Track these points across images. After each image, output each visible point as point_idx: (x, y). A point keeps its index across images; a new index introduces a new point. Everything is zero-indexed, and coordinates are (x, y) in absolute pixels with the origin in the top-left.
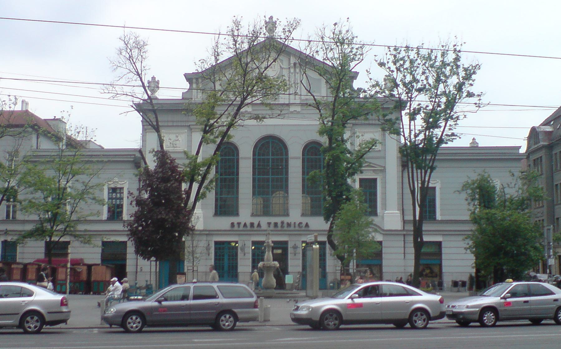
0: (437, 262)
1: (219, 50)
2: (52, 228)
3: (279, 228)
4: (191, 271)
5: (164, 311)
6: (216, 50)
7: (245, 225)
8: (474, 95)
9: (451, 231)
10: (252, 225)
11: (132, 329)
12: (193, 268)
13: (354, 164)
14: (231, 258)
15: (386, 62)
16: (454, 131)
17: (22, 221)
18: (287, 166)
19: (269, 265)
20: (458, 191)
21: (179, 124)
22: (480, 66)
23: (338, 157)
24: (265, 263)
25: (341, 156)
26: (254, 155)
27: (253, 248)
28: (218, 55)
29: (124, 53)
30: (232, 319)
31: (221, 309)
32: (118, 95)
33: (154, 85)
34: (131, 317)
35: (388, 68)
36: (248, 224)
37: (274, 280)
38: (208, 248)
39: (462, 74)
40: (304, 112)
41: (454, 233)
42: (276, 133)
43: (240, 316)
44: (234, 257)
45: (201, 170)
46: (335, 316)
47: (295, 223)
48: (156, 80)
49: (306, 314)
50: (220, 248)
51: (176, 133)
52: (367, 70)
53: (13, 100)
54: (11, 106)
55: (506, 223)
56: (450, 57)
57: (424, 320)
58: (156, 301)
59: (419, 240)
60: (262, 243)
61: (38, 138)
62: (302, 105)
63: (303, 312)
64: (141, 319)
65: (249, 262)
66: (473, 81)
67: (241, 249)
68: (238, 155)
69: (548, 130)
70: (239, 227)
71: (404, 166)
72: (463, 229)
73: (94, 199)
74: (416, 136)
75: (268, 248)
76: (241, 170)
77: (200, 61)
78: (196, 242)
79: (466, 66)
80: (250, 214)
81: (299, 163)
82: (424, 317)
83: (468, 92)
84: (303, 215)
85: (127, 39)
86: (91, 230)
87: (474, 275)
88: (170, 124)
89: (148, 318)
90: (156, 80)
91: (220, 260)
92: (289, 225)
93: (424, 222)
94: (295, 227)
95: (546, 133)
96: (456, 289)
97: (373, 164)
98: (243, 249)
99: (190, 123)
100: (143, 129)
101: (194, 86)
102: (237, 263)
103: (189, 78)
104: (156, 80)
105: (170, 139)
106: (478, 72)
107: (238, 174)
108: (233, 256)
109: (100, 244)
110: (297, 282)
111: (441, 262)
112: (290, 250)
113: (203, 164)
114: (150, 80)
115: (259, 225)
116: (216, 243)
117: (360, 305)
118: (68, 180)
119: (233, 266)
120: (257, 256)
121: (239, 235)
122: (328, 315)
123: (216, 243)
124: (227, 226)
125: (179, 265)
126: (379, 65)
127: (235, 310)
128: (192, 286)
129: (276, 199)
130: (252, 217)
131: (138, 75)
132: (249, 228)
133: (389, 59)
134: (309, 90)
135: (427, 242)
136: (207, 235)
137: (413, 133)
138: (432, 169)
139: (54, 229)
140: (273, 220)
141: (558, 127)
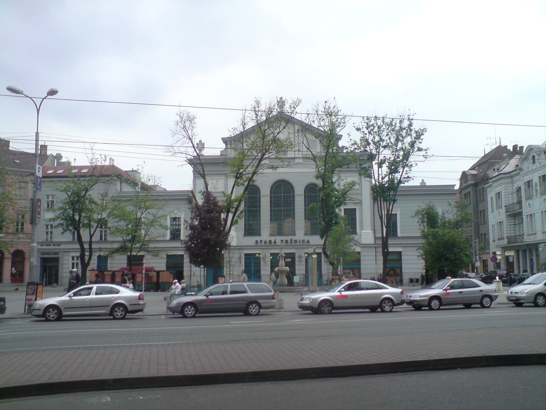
0: (399, 266)
1: (246, 121)
3: (289, 244)
7: (265, 242)
8: (423, 149)
10: (270, 242)
11: (188, 316)
12: (230, 272)
15: (361, 127)
16: (409, 175)
17: (111, 241)
19: (282, 270)
24: (280, 268)
26: (271, 193)
27: (271, 258)
28: (245, 125)
29: (180, 124)
30: (257, 307)
32: (176, 154)
33: (201, 146)
36: (268, 242)
37: (286, 280)
38: (240, 258)
39: (414, 135)
40: (305, 163)
41: (413, 245)
42: (286, 178)
43: (262, 305)
45: (234, 205)
47: (300, 240)
49: (309, 303)
50: (248, 258)
51: (217, 179)
52: (348, 134)
53: (104, 158)
55: (446, 238)
56: (406, 124)
58: (204, 296)
59: (386, 251)
60: (278, 254)
61: (121, 184)
62: (303, 158)
63: (306, 302)
64: (194, 308)
65: (269, 268)
66: (422, 140)
69: (474, 173)
70: (261, 243)
71: (375, 199)
73: (161, 225)
74: (383, 179)
79: (417, 130)
82: (390, 304)
83: (418, 148)
87: (424, 274)
88: (213, 173)
89: (199, 308)
92: (296, 241)
94: (300, 243)
96: (412, 284)
98: (264, 259)
99: (226, 172)
101: (229, 146)
102: (260, 269)
105: (213, 183)
106: (425, 133)
109: (165, 256)
112: (297, 259)
113: (236, 200)
114: (198, 142)
115: (275, 242)
116: (246, 255)
117: (346, 296)
120: (274, 264)
122: (323, 304)
123: (246, 255)
127: (259, 301)
128: (229, 285)
129: (287, 223)
132: (268, 244)
133: (363, 126)
137: (380, 177)
139: (133, 246)
140: (285, 238)
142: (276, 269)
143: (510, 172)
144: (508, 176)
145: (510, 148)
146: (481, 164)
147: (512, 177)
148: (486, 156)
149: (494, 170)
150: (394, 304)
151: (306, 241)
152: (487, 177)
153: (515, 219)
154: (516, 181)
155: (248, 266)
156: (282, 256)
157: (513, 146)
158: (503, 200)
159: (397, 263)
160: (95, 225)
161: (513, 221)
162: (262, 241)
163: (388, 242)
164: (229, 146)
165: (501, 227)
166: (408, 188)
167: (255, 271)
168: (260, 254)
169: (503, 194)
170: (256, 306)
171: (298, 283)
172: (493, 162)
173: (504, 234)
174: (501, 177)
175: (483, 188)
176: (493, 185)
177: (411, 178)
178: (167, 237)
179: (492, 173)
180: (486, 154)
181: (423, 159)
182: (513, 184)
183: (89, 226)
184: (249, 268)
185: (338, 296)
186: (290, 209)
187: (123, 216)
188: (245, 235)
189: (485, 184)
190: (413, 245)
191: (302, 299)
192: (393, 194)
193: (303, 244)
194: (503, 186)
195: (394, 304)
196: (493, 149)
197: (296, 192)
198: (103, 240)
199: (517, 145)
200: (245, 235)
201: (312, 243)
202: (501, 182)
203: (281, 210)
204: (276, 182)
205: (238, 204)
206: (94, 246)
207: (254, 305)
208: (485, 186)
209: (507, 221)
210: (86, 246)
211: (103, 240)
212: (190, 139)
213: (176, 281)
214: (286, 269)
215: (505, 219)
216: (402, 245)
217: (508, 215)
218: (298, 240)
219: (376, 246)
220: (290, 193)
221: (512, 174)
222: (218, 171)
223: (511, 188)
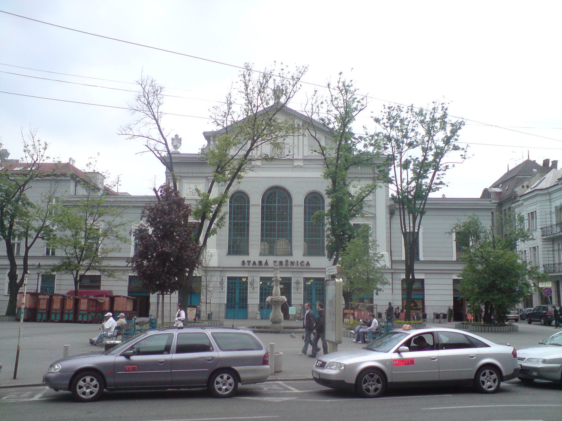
0: (421, 297)
1: (232, 100)
2: (79, 263)
3: (284, 266)
4: (205, 303)
5: (134, 369)
6: (229, 99)
7: (254, 263)
9: (433, 270)
10: (260, 263)
11: (84, 397)
12: (206, 300)
13: (354, 206)
15: (380, 118)
16: (442, 180)
17: (60, 257)
20: (449, 233)
21: (198, 175)
22: (464, 123)
23: (342, 198)
24: (273, 297)
25: (345, 198)
27: (261, 283)
28: (231, 103)
29: (143, 99)
30: (231, 380)
31: (218, 366)
32: (134, 137)
33: (177, 140)
34: (83, 378)
36: (257, 263)
37: (282, 314)
38: (221, 283)
39: (449, 128)
41: (448, 272)
43: (242, 376)
44: (245, 291)
45: (212, 208)
46: (376, 376)
47: (297, 262)
49: (337, 375)
50: (232, 283)
51: (195, 183)
52: (364, 127)
53: (43, 146)
54: (40, 150)
55: (501, 261)
56: (438, 115)
57: (494, 381)
58: (122, 355)
59: (411, 277)
60: (270, 279)
61: (76, 186)
62: (304, 160)
63: (331, 372)
64: (98, 381)
67: (250, 284)
68: (249, 202)
70: (249, 264)
71: (392, 213)
73: (117, 237)
74: (408, 184)
75: (277, 282)
76: (251, 215)
77: (213, 107)
79: (453, 122)
80: (258, 254)
81: (302, 210)
82: (494, 376)
83: (454, 145)
85: (144, 83)
87: (452, 308)
88: (190, 175)
89: (109, 380)
90: (179, 137)
91: (232, 293)
92: (292, 263)
93: (415, 262)
94: (297, 265)
95: (496, 193)
96: (437, 320)
98: (252, 284)
99: (207, 175)
101: (212, 143)
102: (247, 296)
103: (208, 136)
104: (179, 137)
105: (190, 188)
106: (462, 127)
107: (248, 219)
108: (243, 289)
109: (127, 279)
110: (299, 314)
111: (424, 297)
112: (293, 285)
113: (215, 201)
114: (174, 137)
115: (266, 263)
116: (229, 278)
117: (411, 361)
118: (94, 219)
119: (243, 298)
120: (265, 291)
121: (249, 271)
122: (367, 377)
123: (229, 278)
124: (239, 264)
125: (191, 298)
126: (375, 121)
127: (236, 368)
128: (175, 332)
129: (281, 244)
132: (257, 266)
134: (314, 136)
135: (418, 279)
136: (221, 271)
137: (405, 181)
138: (422, 213)
139: (81, 263)
140: (279, 259)
141: (507, 189)
142: (269, 299)
143: (547, 188)
144: (545, 192)
145: (540, 163)
146: (505, 182)
147: (550, 194)
148: (509, 172)
149: (523, 187)
150: (501, 378)
151: (305, 263)
152: (515, 194)
153: (553, 244)
154: (555, 199)
156: (277, 280)
157: (544, 161)
158: (538, 221)
159: (419, 293)
160: (34, 234)
161: (551, 246)
162: (250, 261)
164: (212, 143)
165: (535, 254)
167: (240, 299)
168: (247, 278)
169: (538, 214)
170: (228, 378)
172: (521, 178)
173: (539, 261)
174: (536, 193)
175: (510, 208)
176: (525, 204)
179: (519, 190)
180: (509, 170)
181: (460, 160)
182: (550, 202)
183: (26, 235)
185: (395, 360)
186: (286, 223)
187: (73, 226)
188: (229, 253)
189: (513, 203)
190: (448, 272)
191: (323, 365)
192: (421, 203)
194: (538, 205)
195: (501, 378)
196: (518, 165)
197: (294, 202)
198: (50, 255)
199: (549, 160)
200: (229, 253)
201: (312, 265)
202: (538, 199)
203: (275, 223)
205: (217, 207)
206: (30, 262)
207: (225, 376)
208: (513, 206)
209: (544, 246)
210: (19, 262)
211: (50, 255)
212: (155, 119)
213: (110, 314)
214: (282, 299)
215: (541, 243)
217: (544, 239)
218: (296, 261)
221: (550, 190)
222: (197, 173)
223: (549, 207)
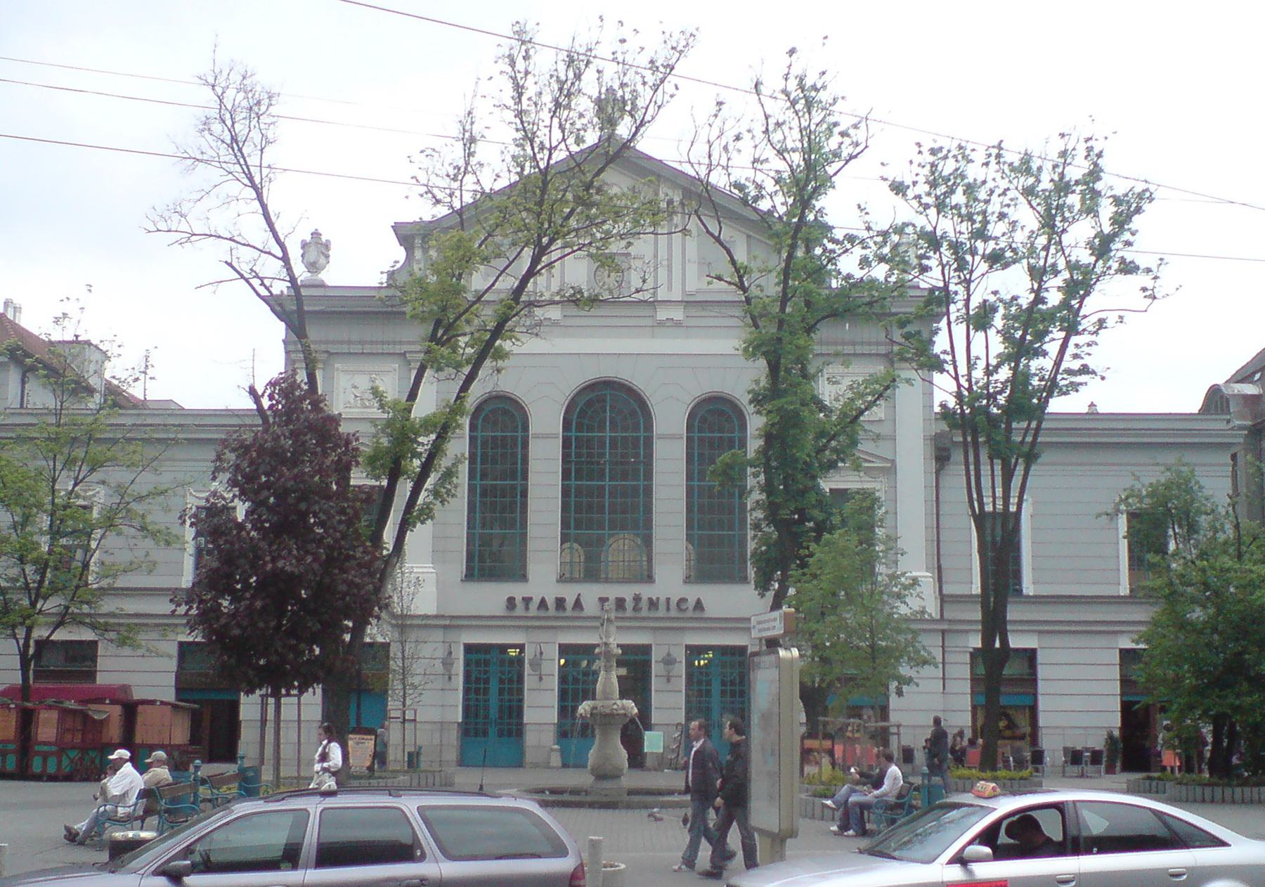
0: (1028, 701)
4: (401, 720)
6: (468, 127)
7: (543, 604)
8: (1137, 268)
9: (1061, 622)
10: (560, 603)
12: (404, 713)
13: (833, 438)
14: (506, 686)
15: (908, 182)
16: (1087, 360)
18: (649, 456)
19: (608, 711)
20: (1107, 514)
21: (379, 349)
22: (1151, 194)
24: (598, 703)
26: (567, 425)
27: (562, 661)
28: (473, 140)
29: (217, 127)
32: (194, 238)
35: (915, 197)
36: (551, 603)
38: (447, 662)
39: (1107, 210)
40: (693, 322)
42: (623, 373)
44: (515, 686)
47: (668, 600)
48: (324, 240)
50: (478, 663)
51: (370, 372)
52: (859, 206)
56: (1075, 172)
59: (997, 645)
60: (587, 650)
61: (23, 383)
62: (687, 304)
65: (552, 699)
66: (1133, 234)
69: (1249, 393)
70: (527, 608)
71: (941, 457)
72: (1123, 618)
74: (989, 372)
77: (422, 152)
78: (413, 645)
79: (1119, 192)
84: (688, 580)
85: (222, 81)
86: (151, 612)
87: (1116, 733)
88: (356, 349)
90: (324, 239)
91: (477, 691)
92: (653, 604)
93: (1009, 599)
94: (668, 609)
96: (1076, 769)
97: (867, 453)
98: (536, 665)
99: (405, 348)
100: (287, 360)
101: (418, 254)
102: (521, 701)
103: (407, 235)
104: (324, 239)
105: (355, 387)
106: (1146, 206)
108: (511, 681)
109: (173, 650)
110: (673, 751)
111: (1036, 701)
112: (656, 668)
113: (427, 425)
114: (308, 238)
115: (578, 604)
116: (469, 649)
123: (469, 649)
124: (499, 608)
126: (892, 190)
128: (314, 806)
129: (619, 547)
130: (561, 584)
131: (254, 186)
132: (552, 611)
133: (917, 175)
134: (717, 234)
135: (1017, 650)
136: (445, 627)
137: (981, 365)
139: (39, 606)
140: (614, 591)
151: (691, 603)
155: (511, 681)
162: (531, 599)
163: (1005, 617)
166: (1064, 420)
168: (521, 647)
171: (660, 757)
177: (1094, 372)
178: (184, 579)
181: (1140, 301)
184: (481, 697)
188: (470, 576)
193: (681, 615)
197: (659, 427)
200: (470, 576)
201: (711, 610)
204: (584, 389)
205: (434, 441)
214: (623, 708)
216: (1035, 628)
218: (663, 599)
219: (945, 627)
220: (636, 428)
222: (377, 343)
